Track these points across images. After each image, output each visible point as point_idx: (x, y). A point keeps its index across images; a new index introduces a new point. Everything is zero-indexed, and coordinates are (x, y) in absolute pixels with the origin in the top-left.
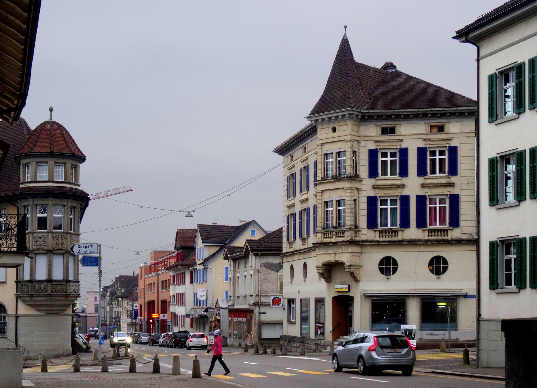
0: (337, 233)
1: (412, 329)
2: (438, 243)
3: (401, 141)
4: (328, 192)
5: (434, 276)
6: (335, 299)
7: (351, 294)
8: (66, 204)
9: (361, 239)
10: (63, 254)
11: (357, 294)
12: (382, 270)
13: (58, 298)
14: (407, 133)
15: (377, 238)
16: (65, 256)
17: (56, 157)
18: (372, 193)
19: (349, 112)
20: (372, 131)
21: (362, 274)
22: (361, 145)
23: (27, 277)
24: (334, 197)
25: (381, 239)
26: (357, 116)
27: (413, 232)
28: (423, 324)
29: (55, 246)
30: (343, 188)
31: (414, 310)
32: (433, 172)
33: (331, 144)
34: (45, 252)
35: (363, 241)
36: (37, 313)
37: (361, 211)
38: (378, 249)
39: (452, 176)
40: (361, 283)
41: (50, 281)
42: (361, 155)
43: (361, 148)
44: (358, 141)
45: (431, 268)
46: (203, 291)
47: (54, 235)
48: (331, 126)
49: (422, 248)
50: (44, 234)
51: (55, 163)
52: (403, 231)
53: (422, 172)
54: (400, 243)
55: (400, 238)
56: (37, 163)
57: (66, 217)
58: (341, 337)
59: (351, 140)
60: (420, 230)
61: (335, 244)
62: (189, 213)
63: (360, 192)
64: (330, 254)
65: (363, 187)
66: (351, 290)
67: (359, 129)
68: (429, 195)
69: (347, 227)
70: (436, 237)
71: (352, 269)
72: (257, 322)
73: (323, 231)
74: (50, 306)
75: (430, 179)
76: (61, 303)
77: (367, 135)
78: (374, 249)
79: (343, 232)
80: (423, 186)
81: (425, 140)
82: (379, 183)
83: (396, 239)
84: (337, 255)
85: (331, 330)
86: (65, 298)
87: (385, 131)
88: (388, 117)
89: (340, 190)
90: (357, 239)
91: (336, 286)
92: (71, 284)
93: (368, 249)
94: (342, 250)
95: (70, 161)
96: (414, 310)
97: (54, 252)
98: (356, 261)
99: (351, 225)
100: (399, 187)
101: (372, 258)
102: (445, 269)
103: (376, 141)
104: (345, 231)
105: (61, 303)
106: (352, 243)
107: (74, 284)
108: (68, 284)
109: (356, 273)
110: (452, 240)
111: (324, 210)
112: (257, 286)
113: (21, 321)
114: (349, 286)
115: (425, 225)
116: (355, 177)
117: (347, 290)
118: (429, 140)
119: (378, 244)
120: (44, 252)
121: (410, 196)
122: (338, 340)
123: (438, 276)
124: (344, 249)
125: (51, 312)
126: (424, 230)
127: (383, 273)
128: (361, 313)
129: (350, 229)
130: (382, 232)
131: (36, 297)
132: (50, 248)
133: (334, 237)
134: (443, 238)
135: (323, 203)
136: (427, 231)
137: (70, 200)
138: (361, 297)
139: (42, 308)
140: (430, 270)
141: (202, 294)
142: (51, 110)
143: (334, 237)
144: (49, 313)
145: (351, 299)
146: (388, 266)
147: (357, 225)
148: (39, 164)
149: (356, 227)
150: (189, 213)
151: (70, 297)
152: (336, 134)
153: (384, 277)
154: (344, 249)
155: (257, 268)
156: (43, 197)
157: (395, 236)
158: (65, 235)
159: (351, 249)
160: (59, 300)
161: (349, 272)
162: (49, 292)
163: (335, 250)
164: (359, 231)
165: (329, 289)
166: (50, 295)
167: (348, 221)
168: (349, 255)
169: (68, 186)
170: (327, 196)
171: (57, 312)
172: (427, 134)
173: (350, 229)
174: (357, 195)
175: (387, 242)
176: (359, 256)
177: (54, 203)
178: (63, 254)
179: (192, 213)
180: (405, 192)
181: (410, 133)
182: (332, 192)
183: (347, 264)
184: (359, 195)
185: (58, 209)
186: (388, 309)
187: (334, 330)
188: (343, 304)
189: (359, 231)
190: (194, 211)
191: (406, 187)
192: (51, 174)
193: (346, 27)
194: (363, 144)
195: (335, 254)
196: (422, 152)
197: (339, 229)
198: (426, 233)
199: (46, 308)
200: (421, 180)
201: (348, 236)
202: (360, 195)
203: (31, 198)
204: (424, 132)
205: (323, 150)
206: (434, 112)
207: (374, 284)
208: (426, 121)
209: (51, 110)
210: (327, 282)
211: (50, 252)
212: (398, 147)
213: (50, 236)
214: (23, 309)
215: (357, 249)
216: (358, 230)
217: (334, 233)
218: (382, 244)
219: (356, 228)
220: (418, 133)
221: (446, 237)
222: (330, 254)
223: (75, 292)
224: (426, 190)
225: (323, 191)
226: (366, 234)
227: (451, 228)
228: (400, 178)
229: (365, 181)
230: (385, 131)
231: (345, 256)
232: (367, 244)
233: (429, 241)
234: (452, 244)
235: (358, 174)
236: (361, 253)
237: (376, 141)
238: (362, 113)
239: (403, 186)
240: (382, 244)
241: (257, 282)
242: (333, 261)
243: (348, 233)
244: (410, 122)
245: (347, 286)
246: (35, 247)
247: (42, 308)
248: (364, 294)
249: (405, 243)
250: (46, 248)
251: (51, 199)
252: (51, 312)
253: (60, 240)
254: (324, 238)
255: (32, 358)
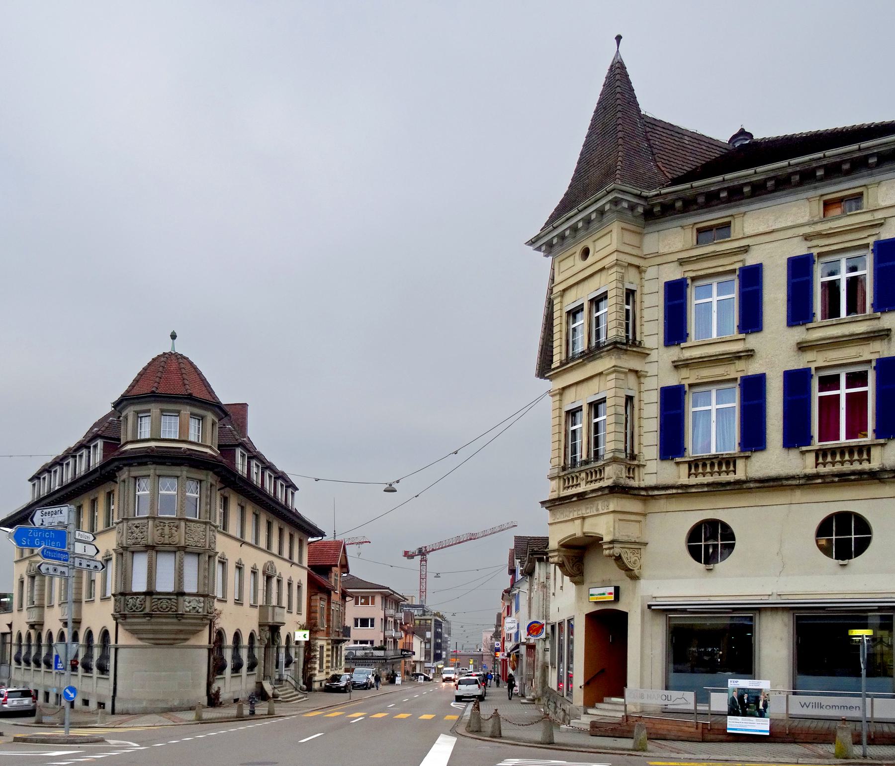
0: (589, 473)
1: (760, 690)
2: (844, 479)
3: (746, 249)
4: (573, 389)
5: (832, 563)
6: (590, 617)
7: (620, 607)
8: (179, 474)
9: (643, 485)
10: (175, 552)
11: (633, 606)
12: (695, 553)
13: (164, 620)
14: (762, 229)
15: (684, 480)
16: (178, 554)
17: (161, 402)
18: (672, 380)
19: (610, 197)
20: (675, 240)
21: (646, 563)
22: (647, 276)
23: (139, 585)
24: (582, 397)
25: (693, 481)
26: (632, 207)
27: (775, 459)
28: (802, 679)
29: (157, 539)
30: (601, 374)
31: (774, 645)
32: (832, 310)
33: (581, 286)
34: (143, 549)
35: (646, 489)
36: (140, 643)
37: (644, 423)
38: (684, 504)
39: (883, 312)
40: (642, 582)
41: (149, 593)
42: (645, 298)
43: (646, 284)
44: (638, 267)
45: (823, 542)
46: (513, 622)
47: (157, 522)
48: (579, 249)
49: (798, 496)
50: (143, 521)
51: (162, 411)
52: (747, 457)
53: (799, 313)
54: (739, 487)
55: (740, 475)
56: (137, 413)
57: (180, 494)
58: (606, 699)
59: (617, 263)
60: (794, 454)
61: (581, 496)
62: (391, 485)
63: (642, 380)
64: (573, 520)
65: (651, 369)
66: (623, 598)
67: (641, 241)
68: (817, 369)
69: (608, 456)
70: (838, 468)
71: (617, 550)
72: (540, 664)
73: (562, 474)
74: (154, 632)
75: (821, 329)
76: (170, 627)
77: (661, 251)
78: (673, 505)
79: (601, 470)
80: (803, 347)
81: (807, 238)
82: (688, 354)
83: (731, 477)
84: (588, 522)
85: (582, 683)
86: (175, 620)
87: (703, 233)
88: (712, 200)
89: (596, 381)
90: (634, 483)
91: (592, 591)
92: (187, 598)
93: (662, 504)
94: (597, 510)
95: (188, 408)
96: (774, 645)
97: (187, 550)
98: (631, 532)
99: (615, 451)
100: (740, 358)
101: (674, 524)
102: (863, 545)
103: (682, 262)
104: (604, 466)
105: (170, 627)
106: (617, 490)
107: (192, 598)
108: (181, 599)
109: (629, 558)
110: (883, 470)
111: (566, 431)
112: (541, 609)
113: (120, 651)
114: (617, 589)
115: (808, 440)
116: (628, 345)
117: (612, 598)
118: (820, 235)
119: (684, 491)
120: (143, 549)
121: (768, 376)
122: (599, 705)
123: (841, 562)
124: (600, 507)
125: (161, 642)
126: (803, 453)
127: (697, 558)
128: (642, 647)
129: (614, 460)
130: (697, 467)
131: (130, 618)
132: (150, 542)
133: (583, 483)
134: (857, 467)
135: (563, 414)
136: (813, 455)
137: (185, 468)
138: (643, 612)
139: (145, 636)
140: (821, 548)
141: (512, 625)
142: (174, 336)
143: (583, 483)
144: (158, 643)
145: (623, 617)
146: (710, 543)
147: (636, 452)
148: (140, 415)
149: (633, 457)
150: (391, 485)
151: (186, 618)
152: (591, 259)
153: (702, 566)
154: (601, 506)
155: (542, 580)
156: (140, 464)
157: (727, 473)
158: (177, 522)
159: (614, 504)
160: (167, 624)
161: (610, 556)
162: (147, 610)
163: (583, 510)
164: (639, 466)
165: (579, 597)
166: (149, 615)
167: (610, 444)
168: (611, 517)
169: (184, 446)
170: (571, 401)
171: (172, 642)
172: (816, 223)
173: (614, 460)
174: (636, 388)
175: (708, 485)
176: (639, 522)
177: (158, 472)
178: (175, 552)
179: (395, 486)
180: (753, 368)
181: (767, 230)
182: (579, 388)
183: (606, 539)
184: (640, 387)
185: (168, 482)
186: (711, 644)
187: (587, 684)
188: (608, 627)
189: (639, 466)
190: (398, 482)
191: (758, 355)
192: (184, 429)
193: (619, 38)
194: (651, 273)
195: (584, 518)
196: (800, 268)
197: (593, 465)
198: (811, 459)
199: (151, 636)
200: (800, 333)
201: (612, 474)
202: (643, 388)
203: (154, 463)
204: (806, 219)
205: (565, 304)
206: (833, 160)
207: (676, 581)
208: (811, 194)
209: (174, 336)
210: (576, 583)
211: (151, 549)
212: (737, 266)
213: (151, 523)
214: (124, 638)
215: (633, 505)
216: (636, 462)
217: (583, 475)
218: (694, 490)
219: (631, 459)
220: (789, 224)
221: (866, 466)
222: (573, 520)
223: (197, 612)
224: (810, 356)
225: (564, 389)
226: (656, 471)
227: (882, 441)
228: (742, 336)
229: (654, 356)
230: (703, 233)
231: (602, 522)
232: (656, 493)
233: (817, 476)
234: (882, 481)
235: (638, 339)
236: (645, 515)
237: (682, 262)
238: (646, 198)
239: (749, 354)
240: (694, 490)
241: (541, 603)
242: (579, 534)
243: (609, 471)
244: (769, 203)
245: (612, 590)
246: (130, 542)
247: (145, 636)
248: (649, 606)
249: (752, 485)
250: (143, 542)
251: (152, 467)
252: (161, 642)
253: (167, 529)
254: (564, 488)
255: (131, 712)
